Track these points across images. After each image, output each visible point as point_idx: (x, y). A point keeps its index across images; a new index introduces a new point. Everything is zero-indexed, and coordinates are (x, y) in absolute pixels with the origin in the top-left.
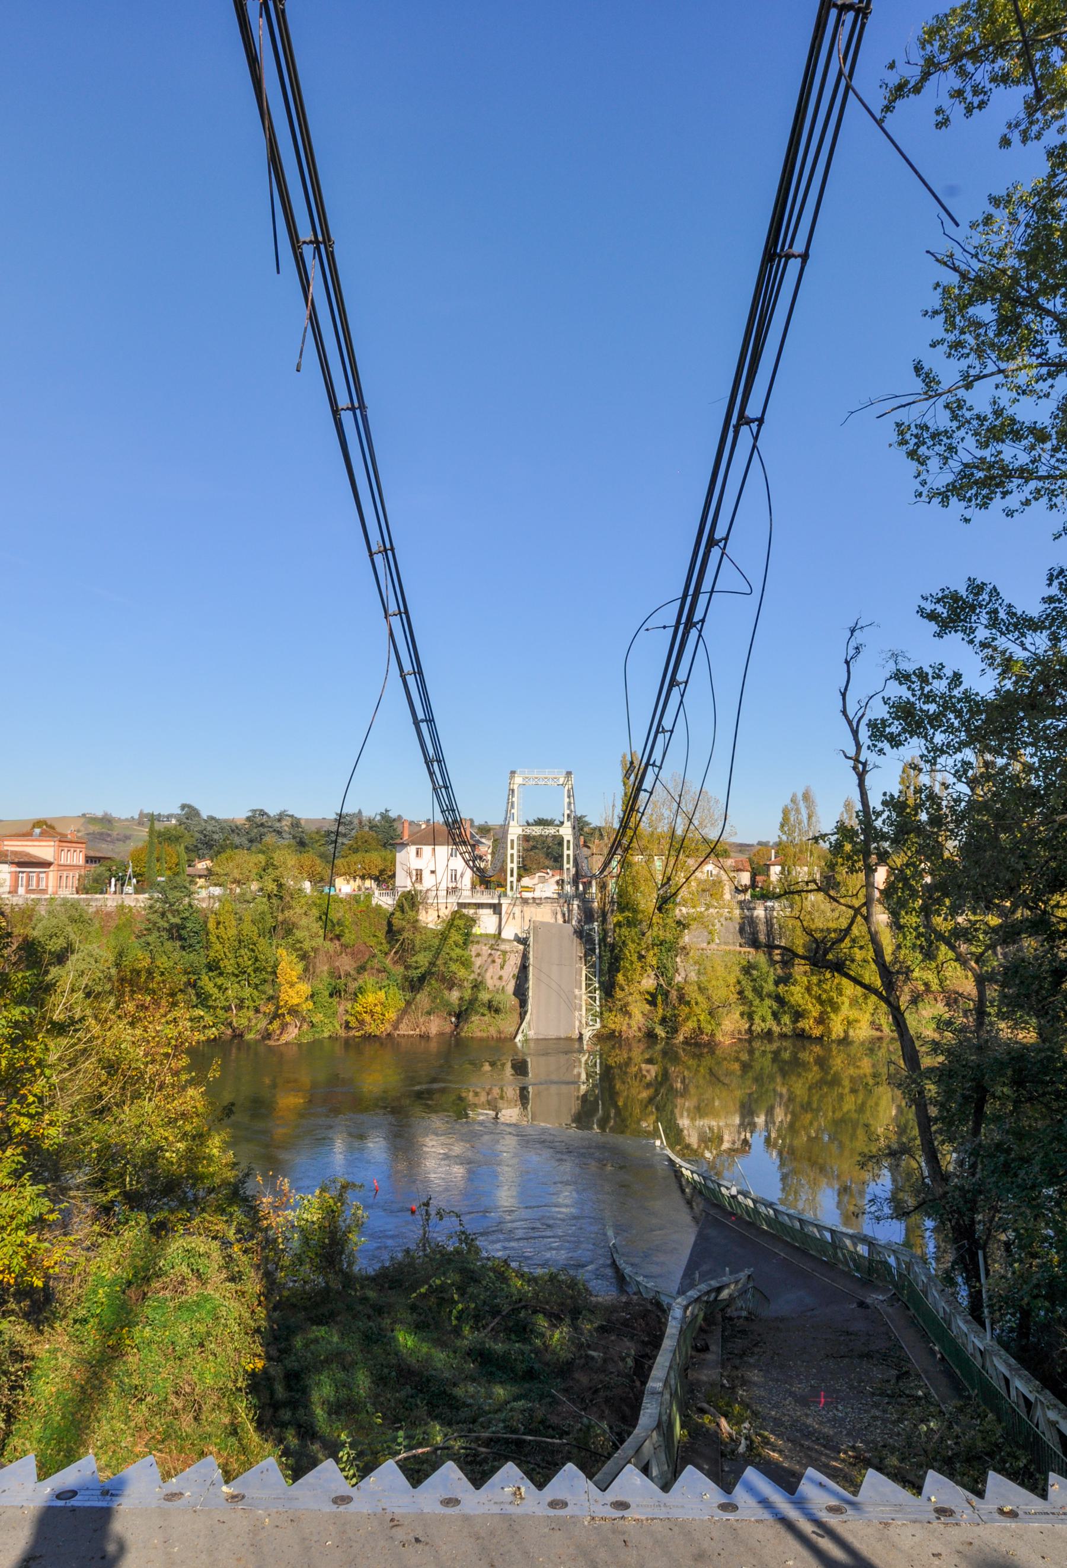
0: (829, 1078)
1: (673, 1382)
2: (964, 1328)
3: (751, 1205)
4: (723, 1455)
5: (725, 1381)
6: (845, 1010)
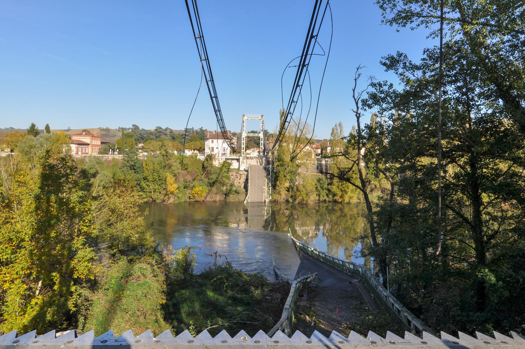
2: (381, 289)
4: (307, 326)
6: (349, 194)
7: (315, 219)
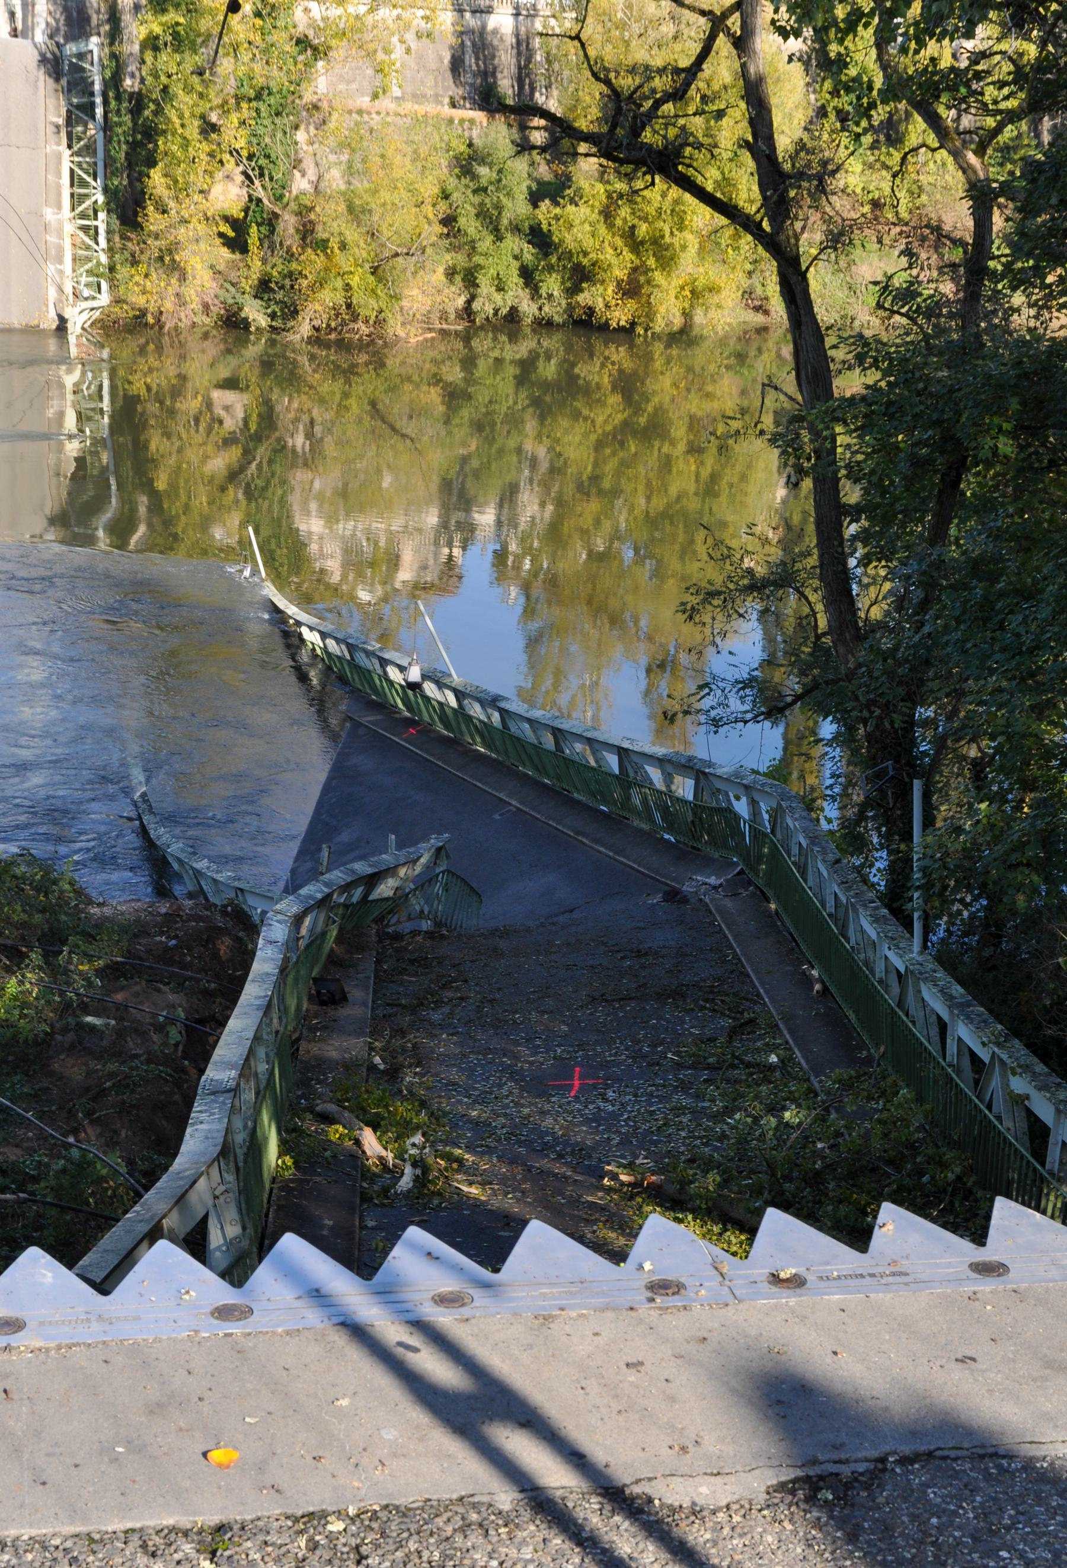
0: (643, 420)
1: (262, 1067)
2: (872, 932)
3: (453, 702)
4: (365, 1198)
5: (377, 1060)
6: (689, 264)
7: (438, 458)
